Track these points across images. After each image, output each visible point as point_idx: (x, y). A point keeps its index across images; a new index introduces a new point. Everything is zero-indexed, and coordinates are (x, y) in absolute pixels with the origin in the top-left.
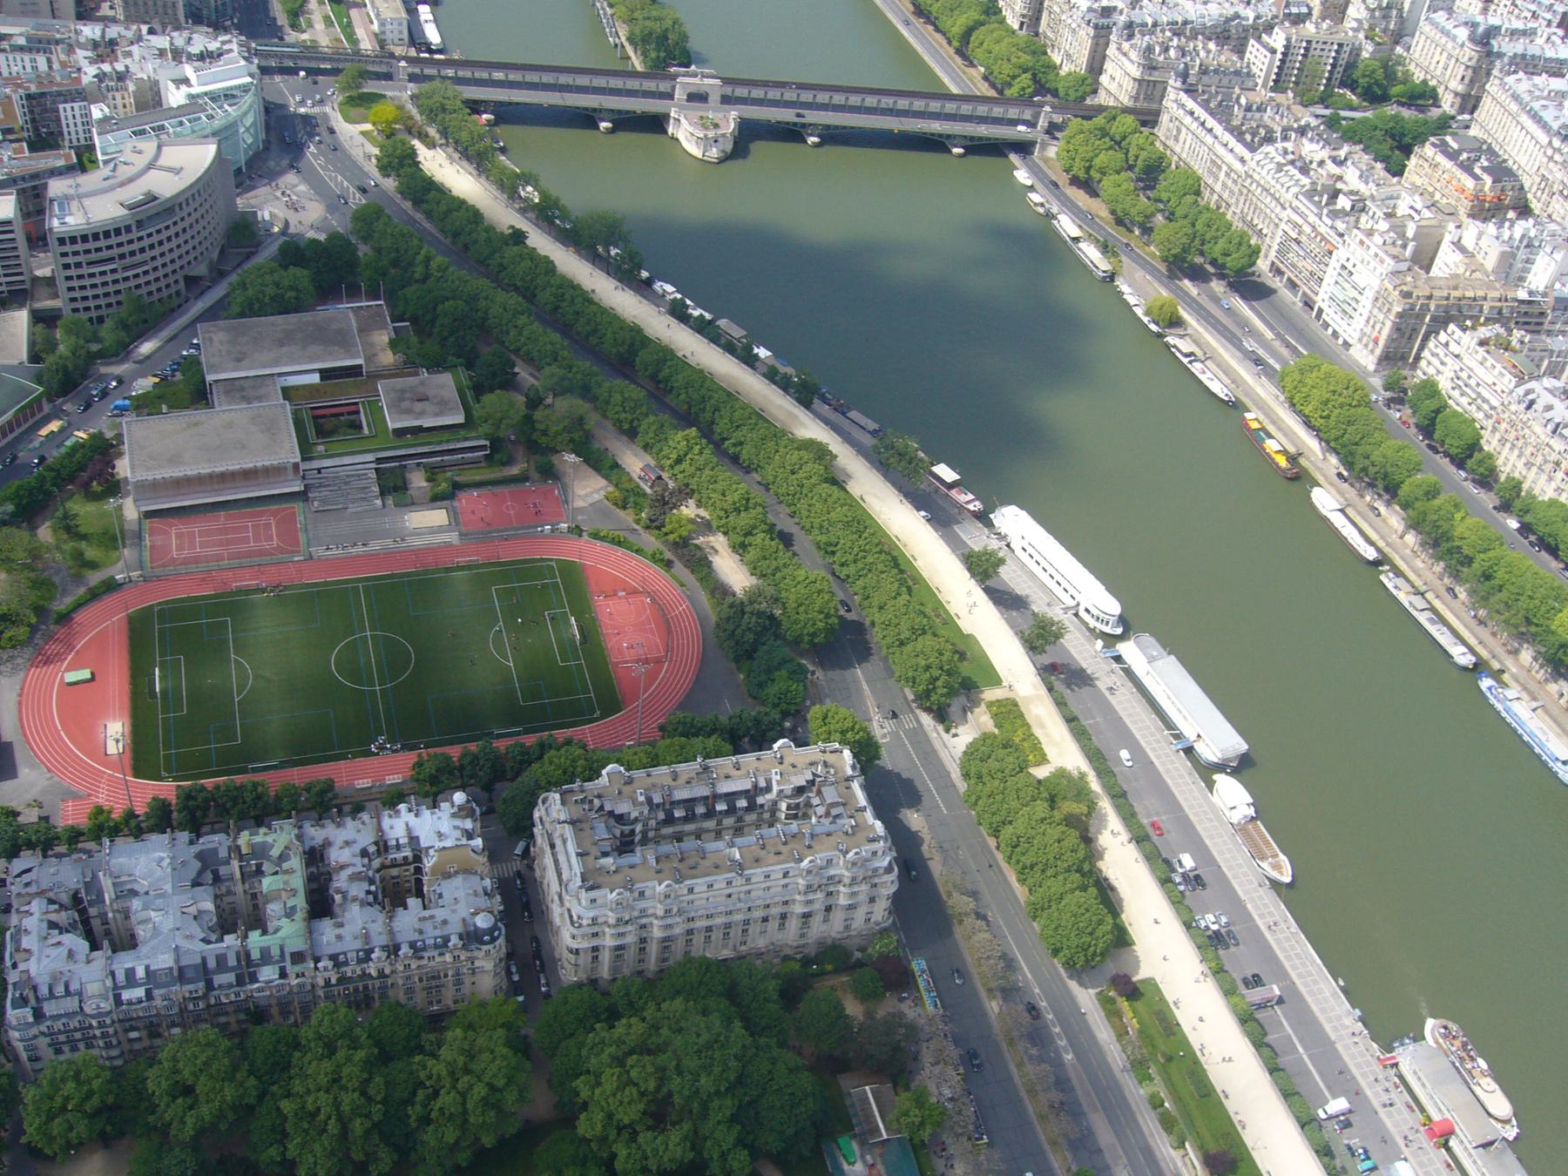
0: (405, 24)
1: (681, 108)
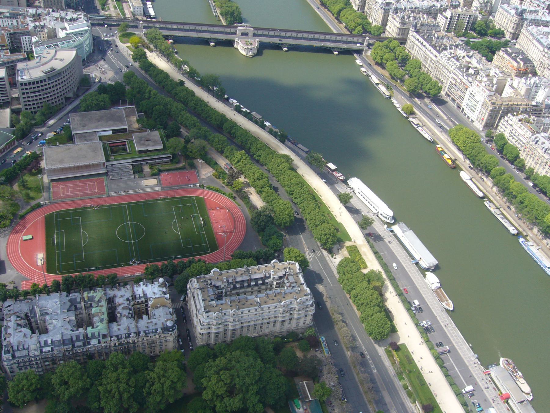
0: (142, 8)
1: (239, 38)
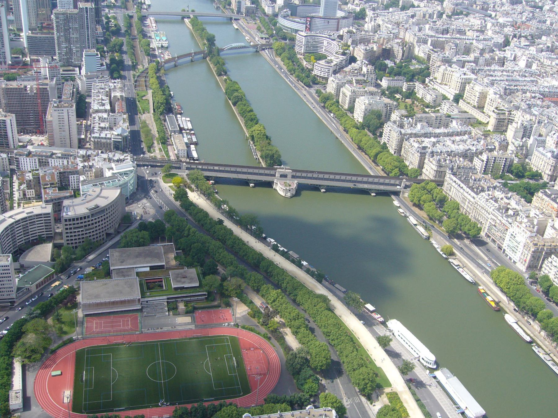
1: (278, 179)
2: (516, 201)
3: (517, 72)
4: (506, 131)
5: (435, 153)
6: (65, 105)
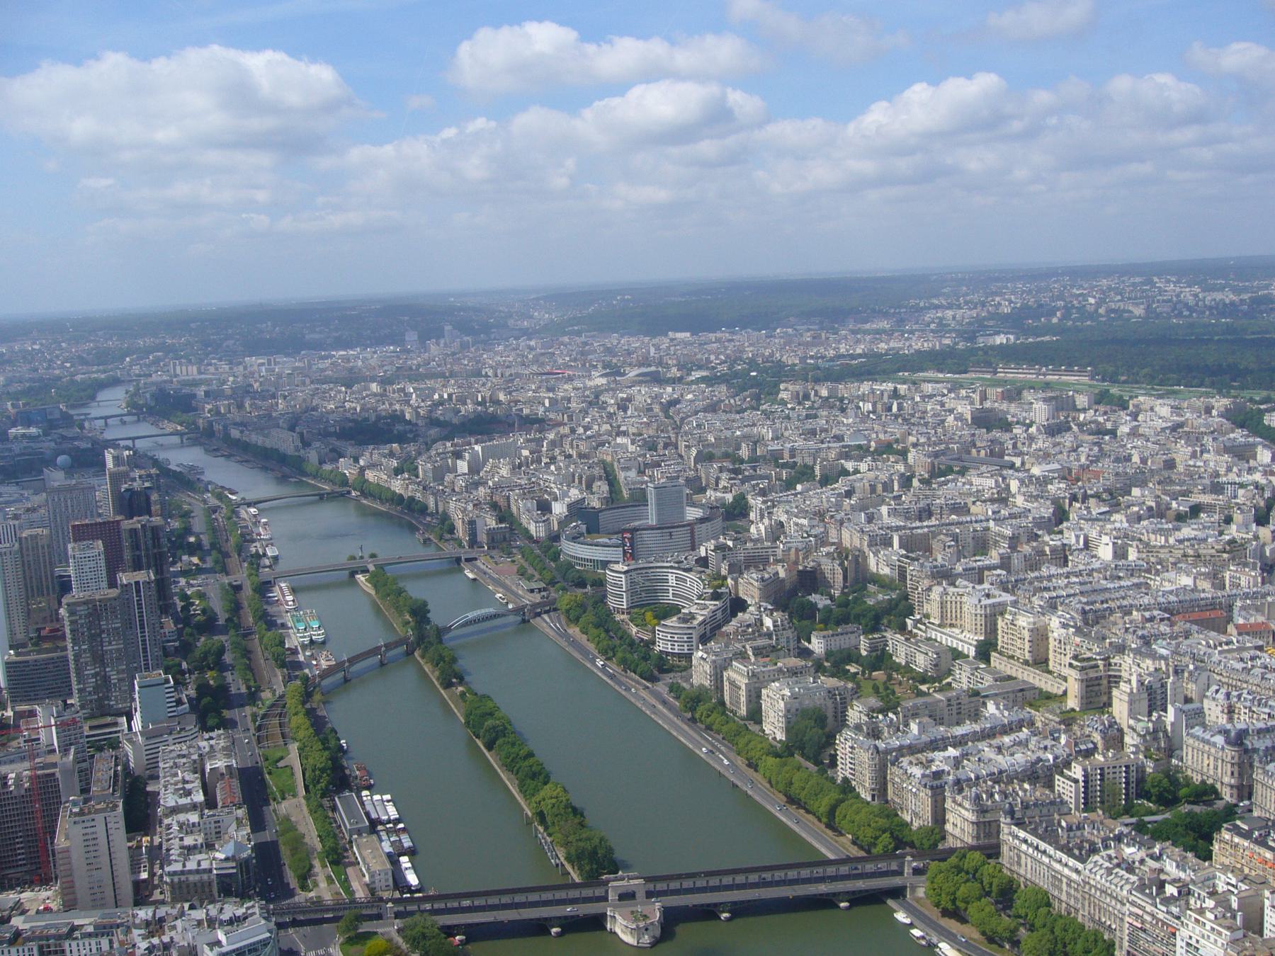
0: (390, 874)
1: (615, 907)
2: (1176, 861)
3: (1100, 572)
4: (1110, 705)
5: (965, 781)
6: (98, 807)
